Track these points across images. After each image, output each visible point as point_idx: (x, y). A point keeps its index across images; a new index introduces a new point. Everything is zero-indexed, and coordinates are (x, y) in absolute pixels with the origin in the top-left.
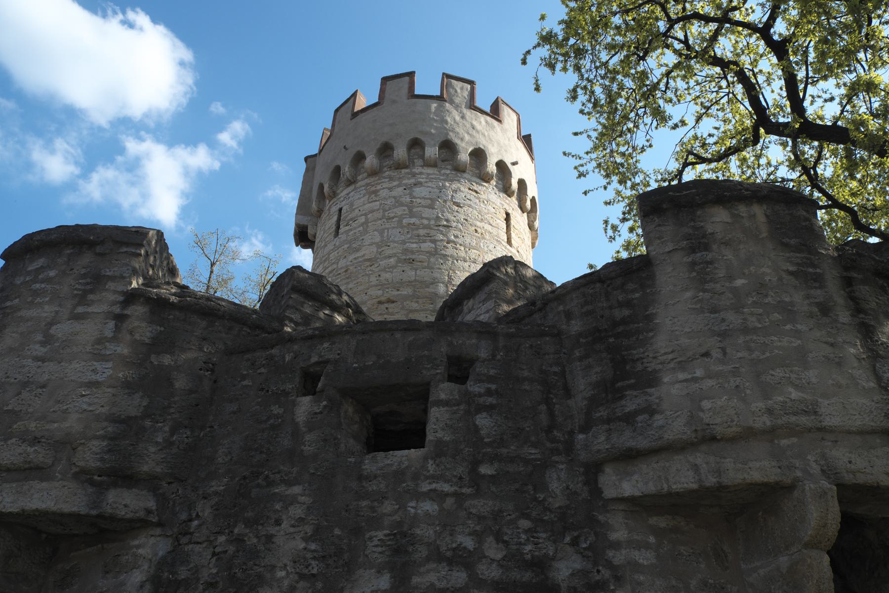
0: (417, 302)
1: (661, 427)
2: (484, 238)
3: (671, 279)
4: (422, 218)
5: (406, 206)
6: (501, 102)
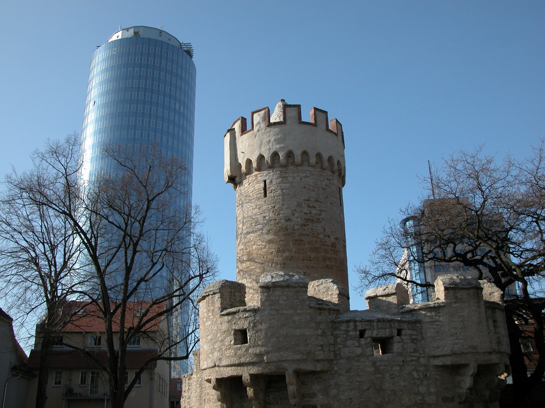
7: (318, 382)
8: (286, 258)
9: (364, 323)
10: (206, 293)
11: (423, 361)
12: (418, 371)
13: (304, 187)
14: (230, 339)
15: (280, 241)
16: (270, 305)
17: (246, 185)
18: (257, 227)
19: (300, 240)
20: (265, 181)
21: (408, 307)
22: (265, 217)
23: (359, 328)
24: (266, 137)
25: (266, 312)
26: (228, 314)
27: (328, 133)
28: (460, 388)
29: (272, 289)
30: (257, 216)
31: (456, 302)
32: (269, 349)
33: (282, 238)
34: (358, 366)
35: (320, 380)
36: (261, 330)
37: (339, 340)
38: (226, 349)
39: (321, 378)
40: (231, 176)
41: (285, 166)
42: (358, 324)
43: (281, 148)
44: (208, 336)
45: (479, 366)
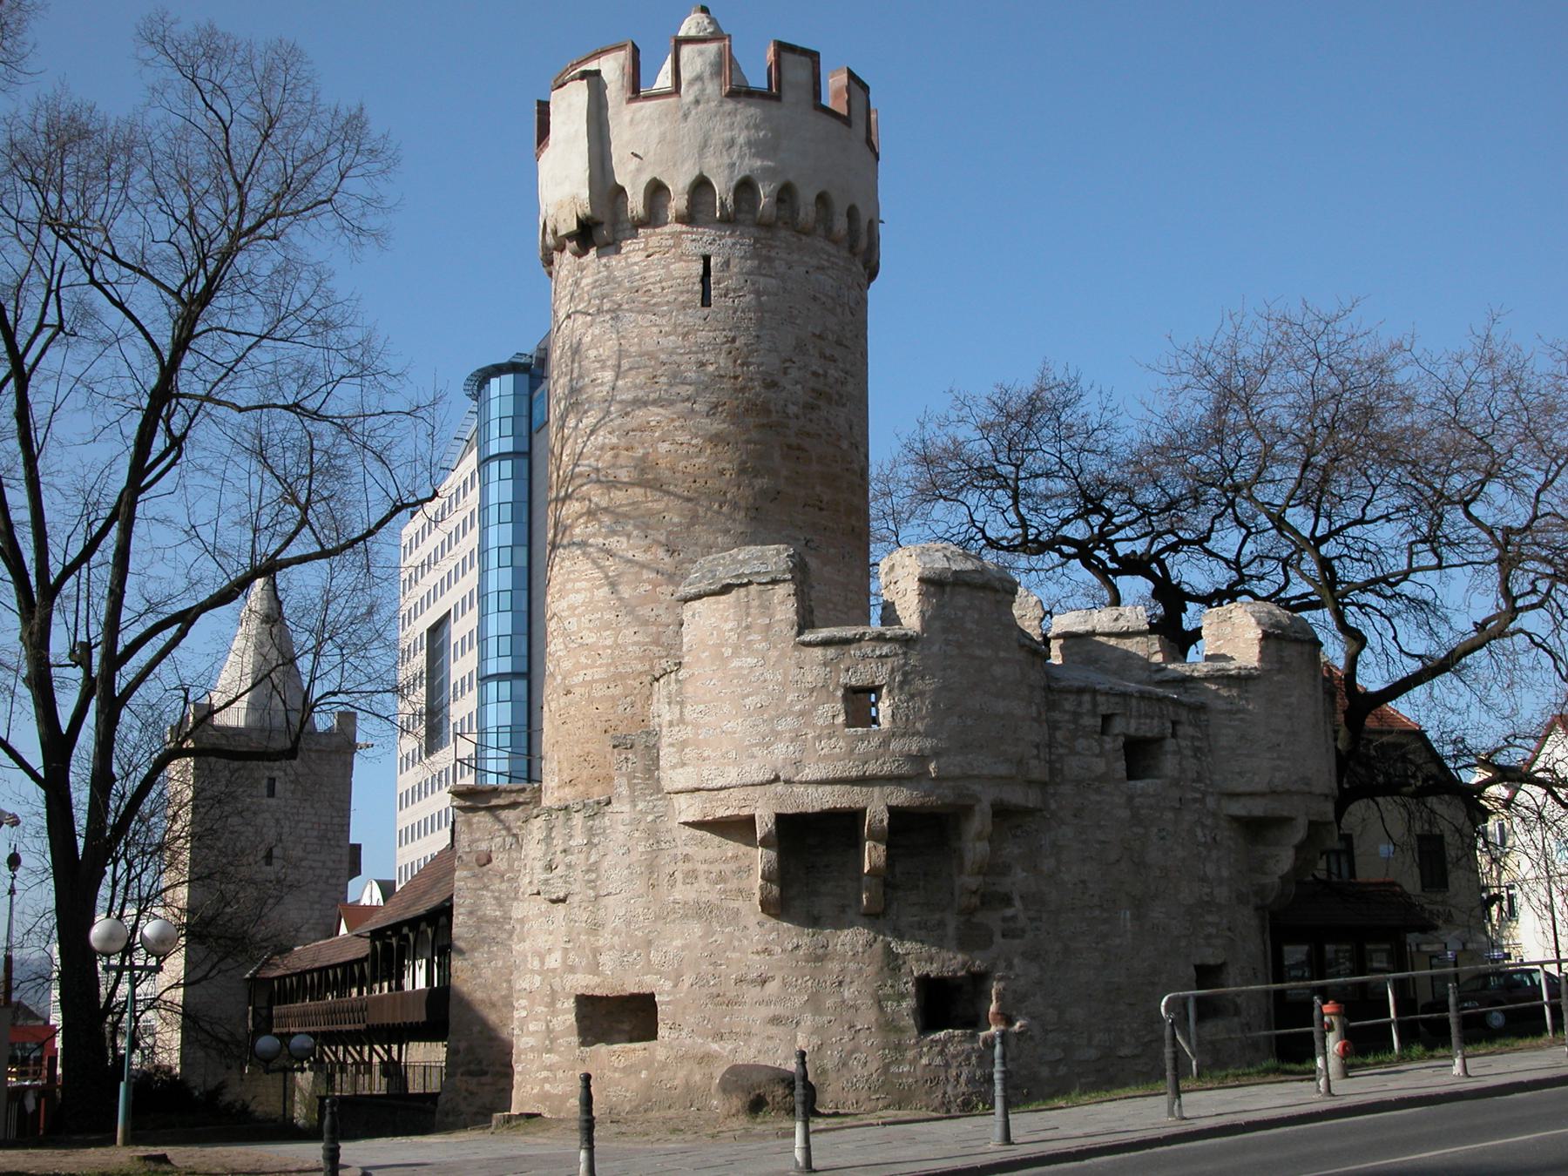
7: (1015, 836)
8: (763, 492)
9: (1113, 700)
10: (738, 576)
11: (1211, 802)
12: (1203, 826)
13: (815, 299)
14: (833, 710)
15: (748, 442)
16: (945, 630)
17: (638, 257)
18: (675, 390)
19: (799, 448)
20: (706, 259)
21: (1174, 670)
22: (702, 364)
23: (1103, 709)
24: (719, 127)
25: (935, 649)
26: (826, 643)
28: (1265, 873)
29: (948, 589)
30: (675, 357)
31: (1279, 671)
32: (943, 745)
33: (755, 435)
34: (1098, 803)
35: (1019, 832)
36: (922, 694)
37: (1059, 735)
38: (819, 738)
39: (1019, 826)
40: (588, 218)
43: (765, 170)
44: (748, 696)
45: (780, 818)
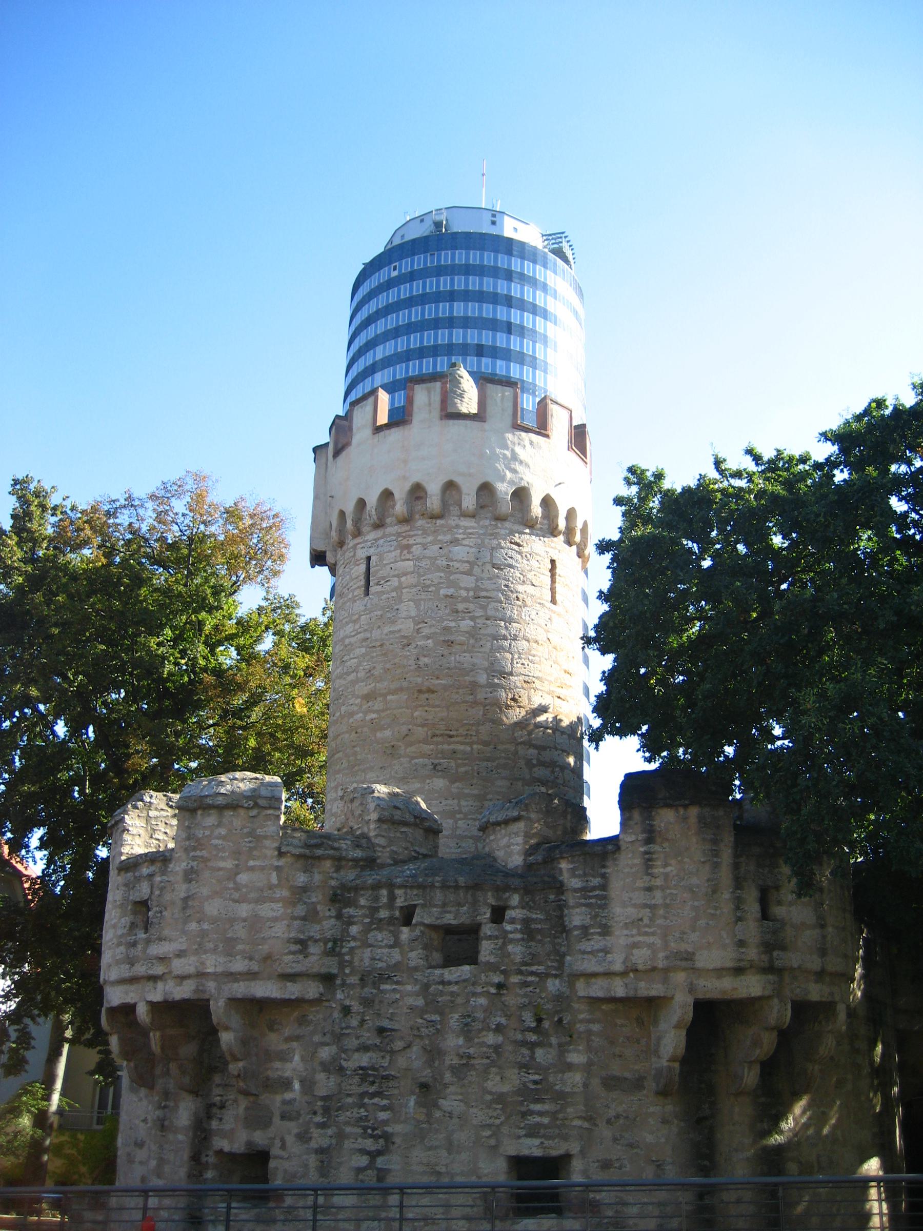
0: (457, 693)
1: (610, 962)
2: (525, 606)
3: (628, 862)
4: (461, 588)
5: (443, 571)
6: (549, 402)
23: (400, 902)
27: (570, 408)
41: (406, 520)
42: (399, 892)
